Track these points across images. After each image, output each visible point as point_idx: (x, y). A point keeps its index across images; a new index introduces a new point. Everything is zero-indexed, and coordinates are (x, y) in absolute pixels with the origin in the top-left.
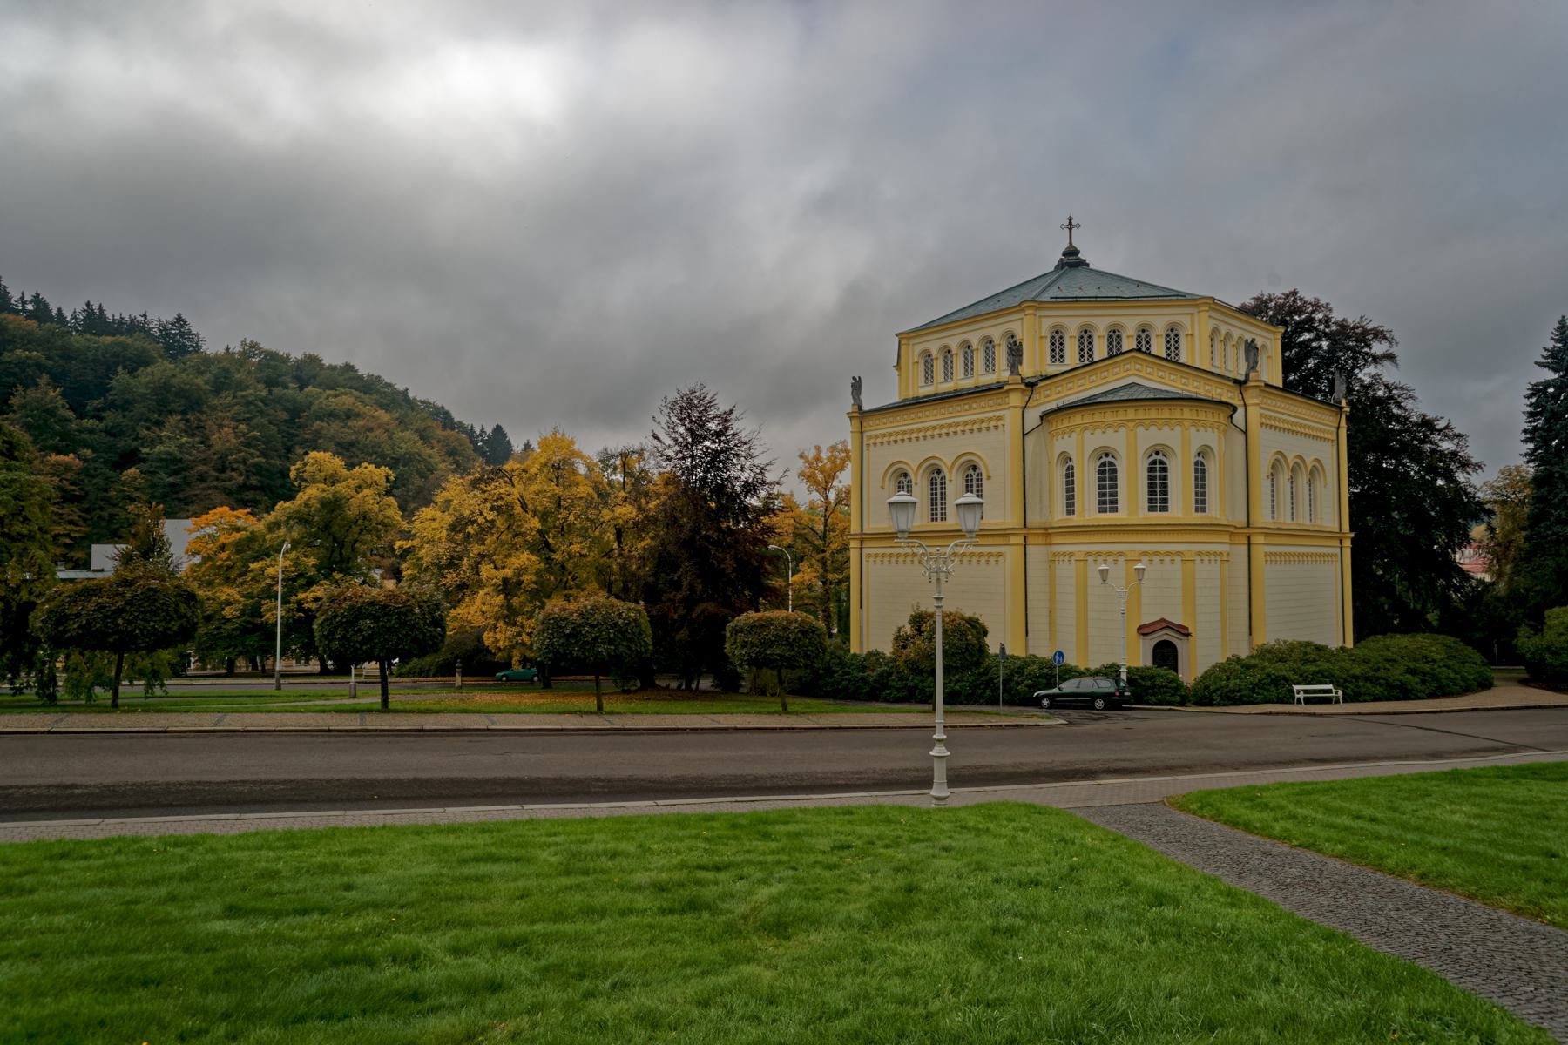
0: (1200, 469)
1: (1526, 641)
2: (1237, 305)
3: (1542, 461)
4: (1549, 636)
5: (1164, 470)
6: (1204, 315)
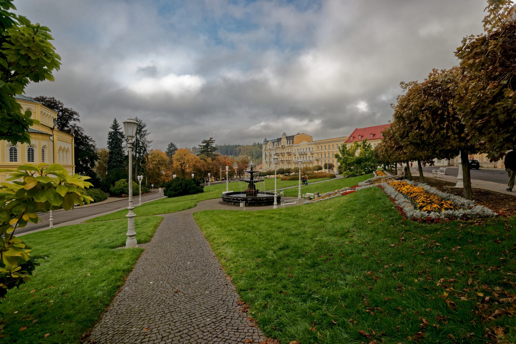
0: (43, 151)
1: (112, 189)
2: (35, 97)
3: (110, 149)
4: (116, 187)
5: (33, 151)
6: (39, 108)
